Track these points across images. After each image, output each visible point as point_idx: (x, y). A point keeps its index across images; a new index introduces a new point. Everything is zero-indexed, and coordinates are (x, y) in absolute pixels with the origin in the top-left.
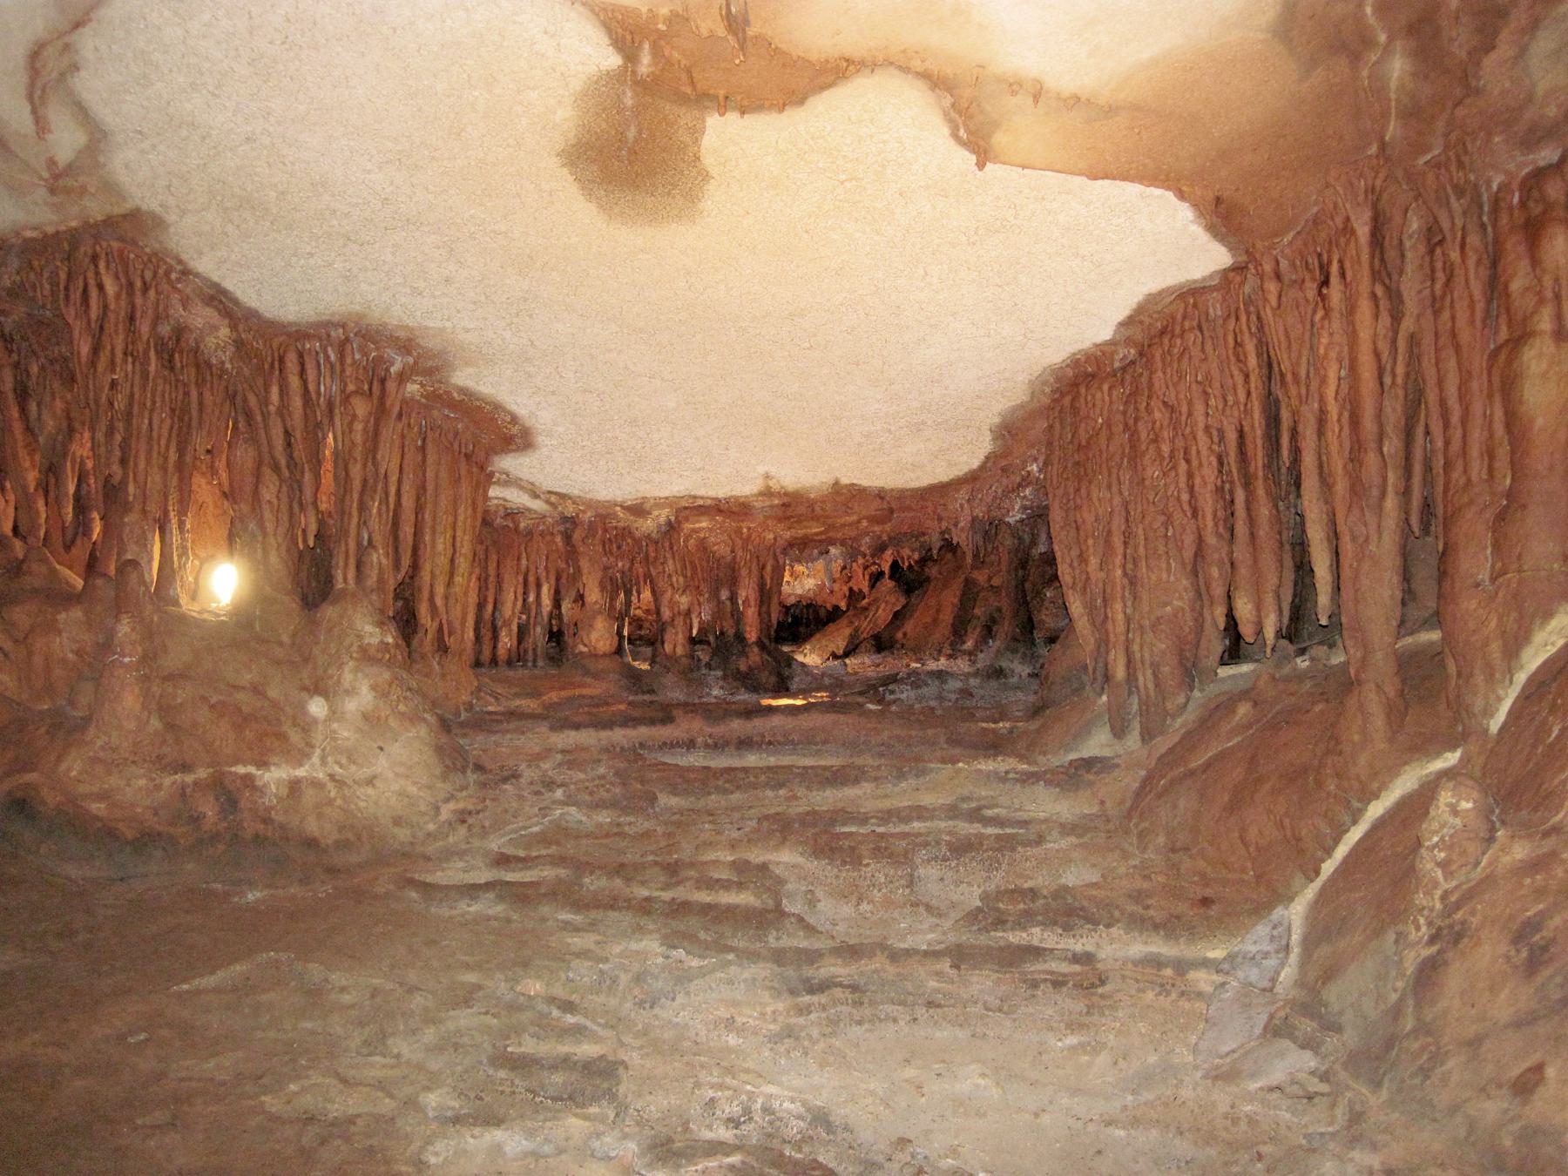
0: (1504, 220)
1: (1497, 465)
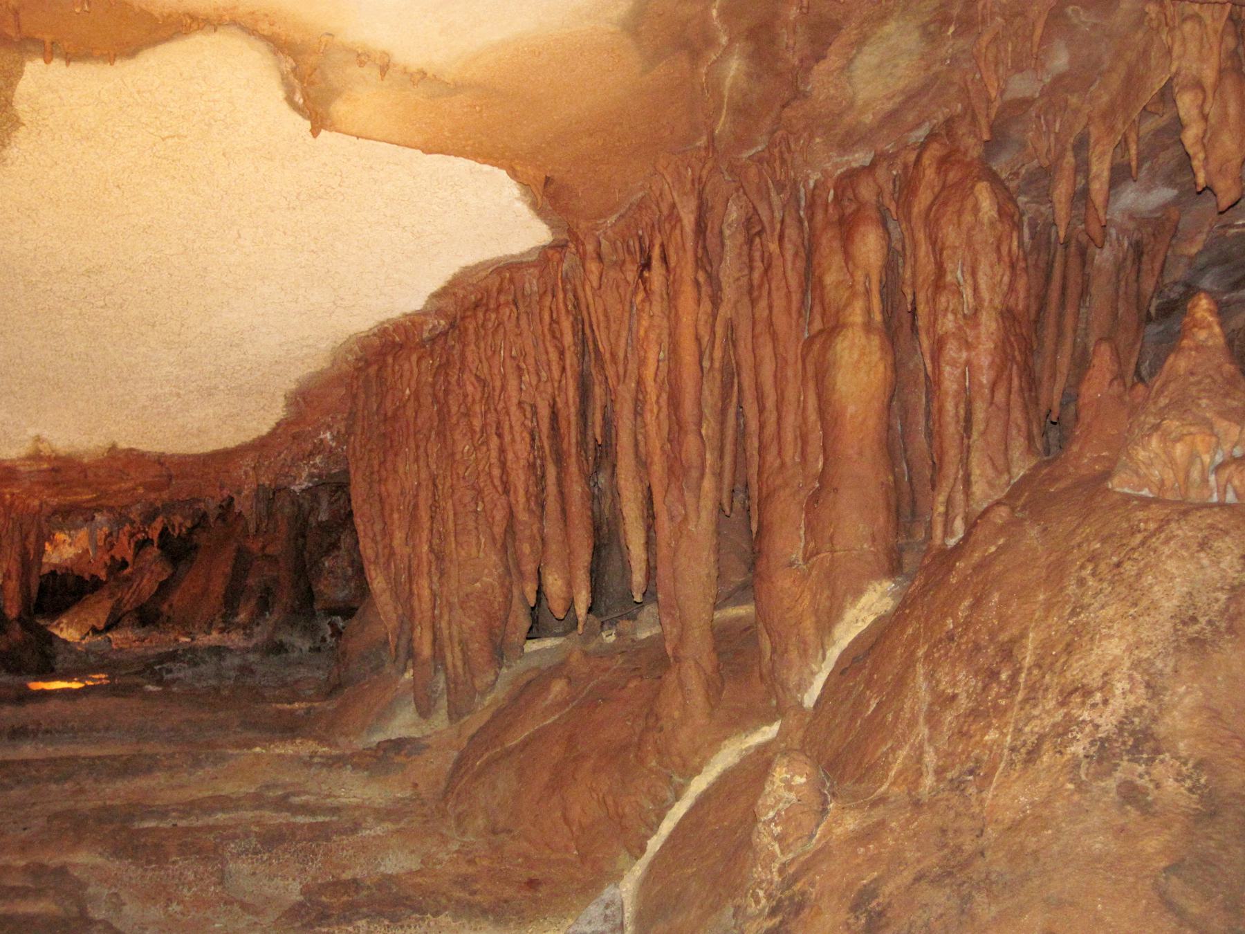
0: (819, 216)
1: (809, 449)
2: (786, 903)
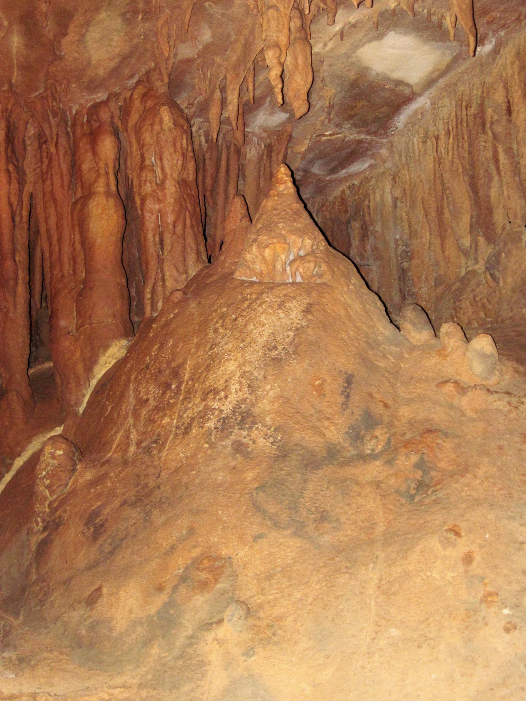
0: (79, 130)
2: (51, 524)
